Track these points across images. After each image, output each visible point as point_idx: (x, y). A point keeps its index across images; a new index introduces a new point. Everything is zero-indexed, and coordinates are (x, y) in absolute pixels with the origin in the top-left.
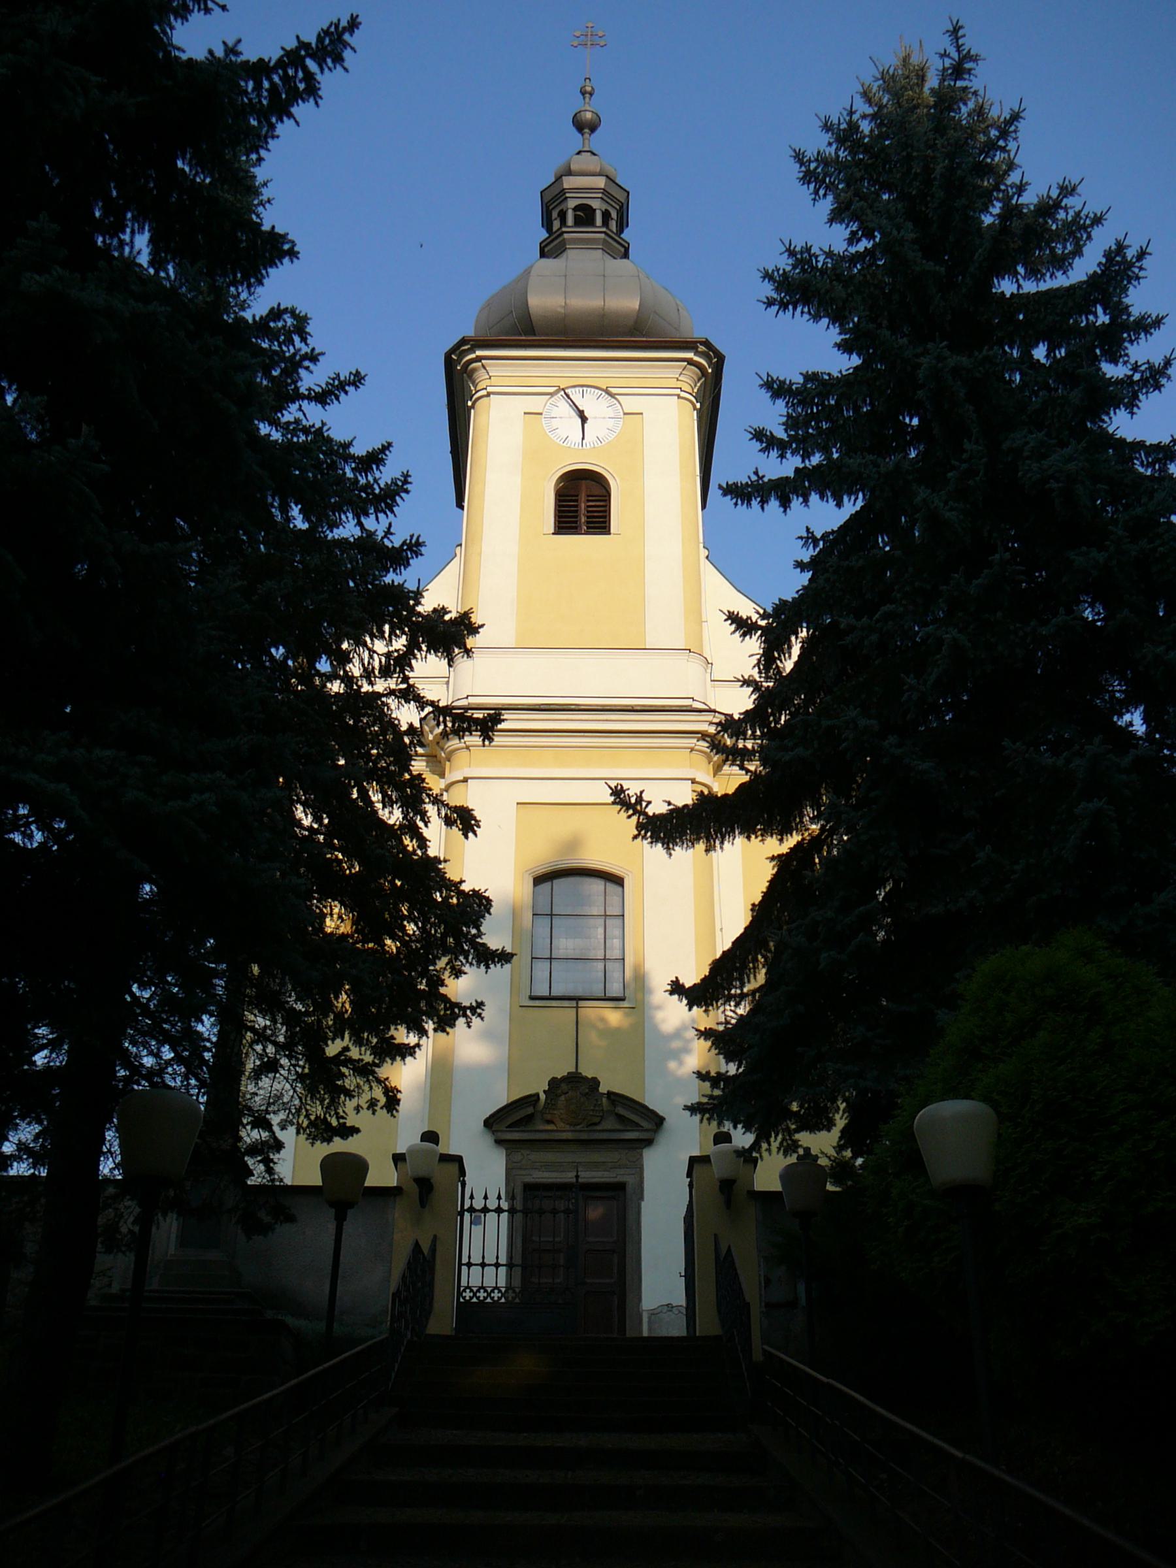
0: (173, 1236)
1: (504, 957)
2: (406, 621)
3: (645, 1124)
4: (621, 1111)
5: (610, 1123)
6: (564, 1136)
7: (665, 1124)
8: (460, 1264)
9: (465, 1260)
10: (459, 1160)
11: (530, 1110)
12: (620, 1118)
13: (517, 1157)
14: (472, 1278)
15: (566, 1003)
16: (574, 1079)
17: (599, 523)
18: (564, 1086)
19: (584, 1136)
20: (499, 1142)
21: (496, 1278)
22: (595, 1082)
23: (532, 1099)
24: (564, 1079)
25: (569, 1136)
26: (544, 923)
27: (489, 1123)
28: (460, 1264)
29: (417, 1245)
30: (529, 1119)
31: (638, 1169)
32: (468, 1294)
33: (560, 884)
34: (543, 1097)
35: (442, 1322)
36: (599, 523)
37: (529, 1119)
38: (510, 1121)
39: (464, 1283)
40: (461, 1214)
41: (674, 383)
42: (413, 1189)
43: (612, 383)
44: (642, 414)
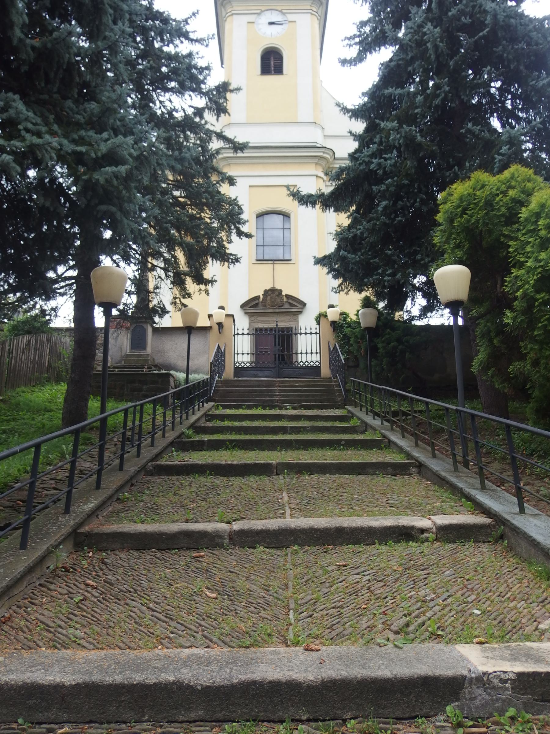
0: (128, 347)
1: (249, 236)
2: (218, 230)
3: (300, 306)
4: (290, 301)
5: (287, 306)
6: (269, 311)
7: (307, 306)
8: (320, 353)
9: (236, 352)
10: (232, 316)
11: (257, 302)
12: (290, 304)
13: (253, 319)
14: (239, 358)
15: (270, 262)
16: (273, 290)
17: (279, 70)
18: (270, 293)
19: (277, 311)
20: (246, 313)
21: (247, 359)
22: (281, 291)
23: (257, 298)
24: (270, 290)
25: (272, 311)
26: (260, 232)
27: (242, 306)
28: (320, 353)
29: (219, 347)
30: (257, 305)
31: (297, 322)
32: (238, 365)
33: (266, 218)
34: (262, 297)
35: (229, 373)
36: (279, 70)
37: (257, 305)
38: (250, 305)
39: (236, 360)
40: (234, 336)
41: (309, 7)
42: (216, 327)
43: (283, 8)
44: (295, 22)
